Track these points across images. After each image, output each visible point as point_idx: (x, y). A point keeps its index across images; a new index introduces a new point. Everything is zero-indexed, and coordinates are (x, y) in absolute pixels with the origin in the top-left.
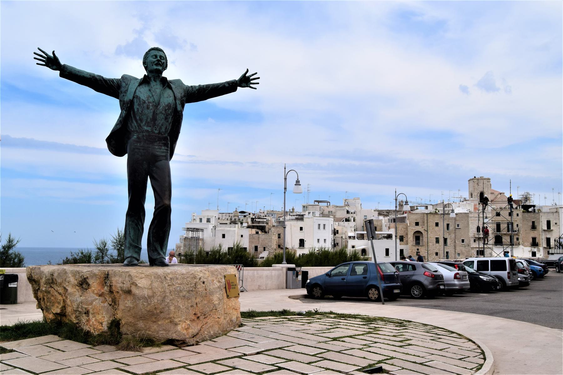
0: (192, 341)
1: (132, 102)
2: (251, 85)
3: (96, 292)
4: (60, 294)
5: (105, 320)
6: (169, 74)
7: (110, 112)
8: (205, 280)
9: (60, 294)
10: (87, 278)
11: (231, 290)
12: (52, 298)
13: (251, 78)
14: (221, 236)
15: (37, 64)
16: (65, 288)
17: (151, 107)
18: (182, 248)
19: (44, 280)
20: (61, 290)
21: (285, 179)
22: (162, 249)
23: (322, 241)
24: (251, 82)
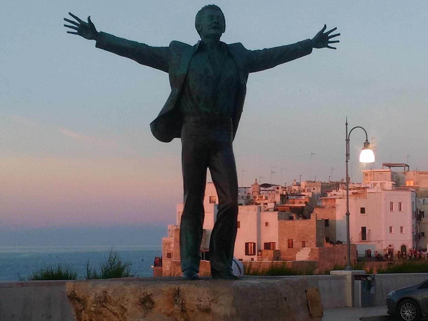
3: (163, 311)
4: (115, 314)
6: (227, 38)
7: (155, 88)
9: (115, 314)
15: (68, 32)
16: (123, 307)
18: (172, 245)
19: (92, 298)
20: (116, 310)
21: (348, 140)
23: (396, 230)
24: (330, 40)
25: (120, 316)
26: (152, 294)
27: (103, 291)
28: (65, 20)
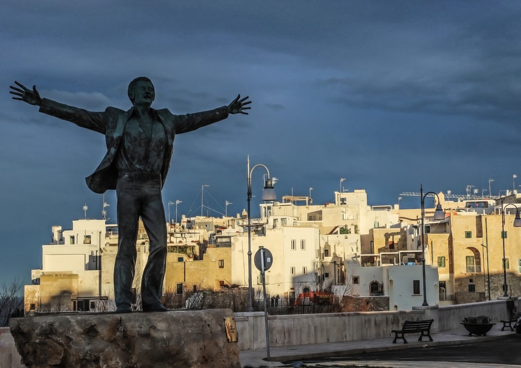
1: (121, 139)
2: (243, 111)
7: (95, 149)
8: (210, 323)
9: (60, 344)
10: (95, 325)
12: (50, 349)
15: (14, 98)
17: (143, 145)
20: (61, 340)
22: (157, 293)
24: (243, 107)
28: (11, 87)
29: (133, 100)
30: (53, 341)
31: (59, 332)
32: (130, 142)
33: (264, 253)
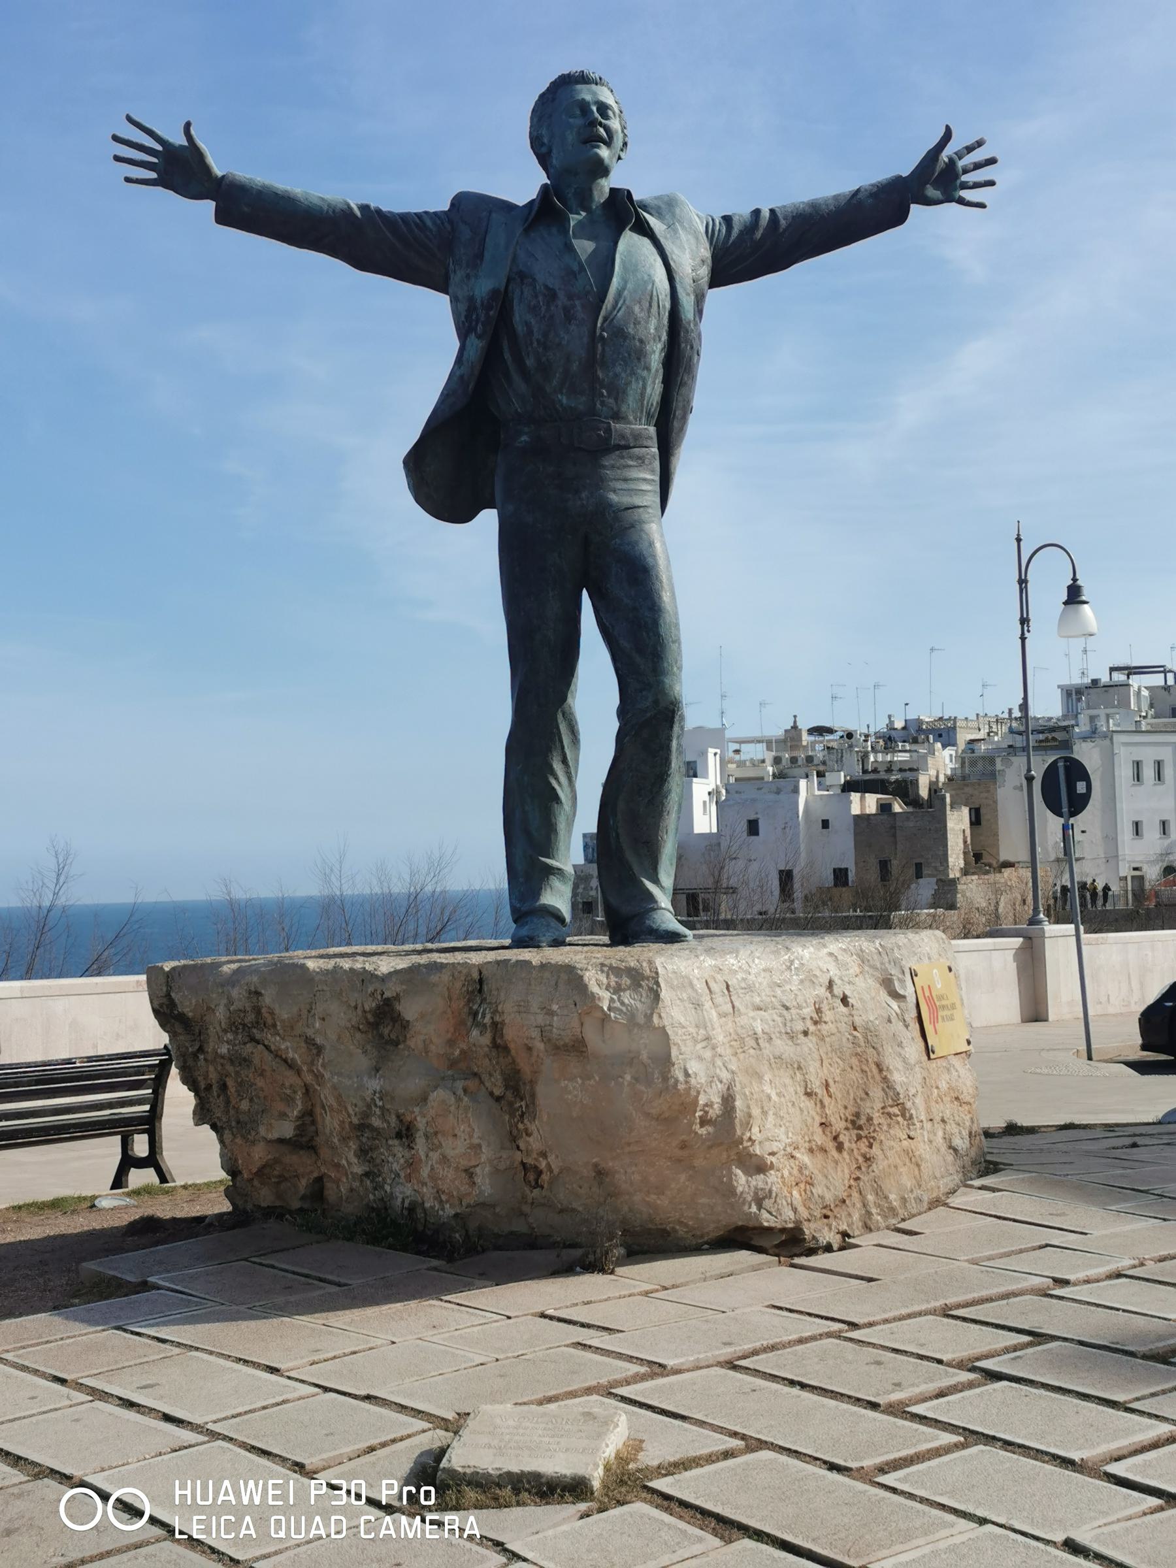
0: (829, 1236)
2: (966, 194)
5: (483, 1158)
7: (414, 343)
9: (290, 1064)
10: (397, 998)
11: (939, 1026)
12: (260, 1083)
13: (961, 164)
14: (744, 826)
15: (128, 180)
16: (309, 1042)
19: (221, 1014)
21: (1023, 582)
24: (964, 178)
25: (305, 1068)
26: (398, 995)
27: (250, 992)
29: (544, 160)
30: (266, 1053)
31: (283, 1021)
32: (534, 310)
33: (1066, 767)
